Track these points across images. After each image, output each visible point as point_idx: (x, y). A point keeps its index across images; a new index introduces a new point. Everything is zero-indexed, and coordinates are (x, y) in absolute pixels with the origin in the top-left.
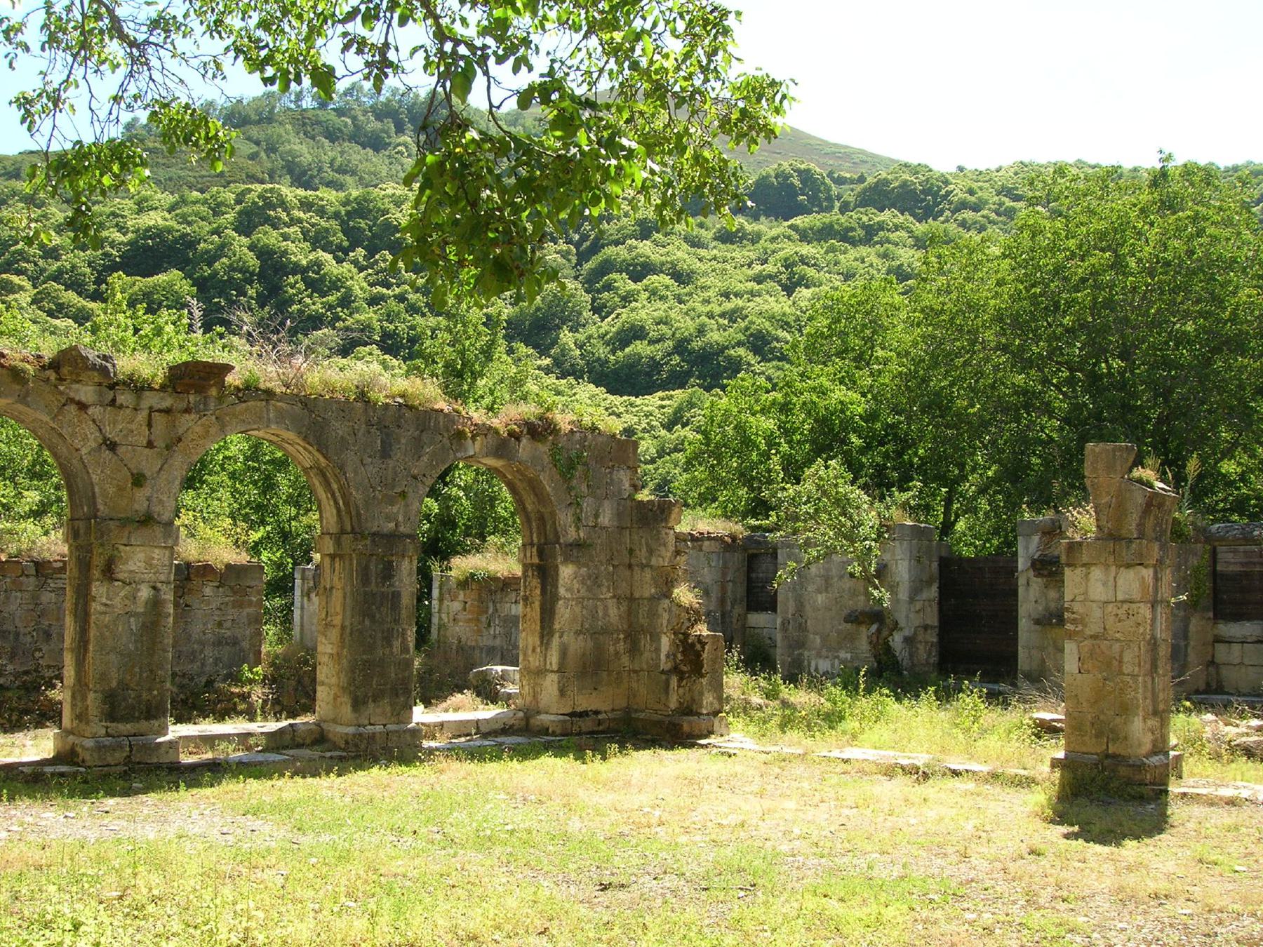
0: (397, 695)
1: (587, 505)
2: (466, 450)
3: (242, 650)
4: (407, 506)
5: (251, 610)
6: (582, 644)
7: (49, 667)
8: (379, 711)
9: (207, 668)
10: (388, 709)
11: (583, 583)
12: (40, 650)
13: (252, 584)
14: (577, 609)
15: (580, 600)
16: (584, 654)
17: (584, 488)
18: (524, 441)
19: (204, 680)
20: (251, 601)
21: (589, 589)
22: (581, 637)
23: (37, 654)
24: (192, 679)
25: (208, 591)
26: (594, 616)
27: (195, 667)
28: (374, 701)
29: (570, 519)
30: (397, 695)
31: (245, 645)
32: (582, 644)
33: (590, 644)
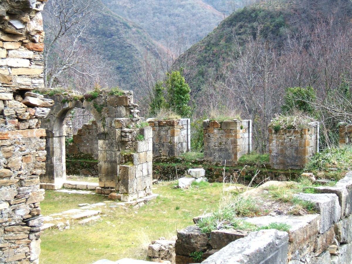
0: (50, 175)
1: (108, 120)
2: (66, 106)
3: (229, 153)
4: (50, 123)
5: (232, 138)
6: (107, 165)
7: (164, 155)
8: (46, 179)
9: (216, 160)
10: (48, 179)
11: (107, 145)
12: (161, 150)
13: (232, 129)
14: (105, 154)
15: (106, 151)
16: (108, 169)
17: (106, 114)
18: (84, 101)
19: (215, 163)
20: (232, 135)
21: (109, 148)
22: (107, 163)
23: (160, 151)
24: (211, 163)
25: (216, 131)
26: (111, 156)
27: (212, 158)
28: (44, 176)
29: (101, 125)
30: (50, 175)
31: (230, 151)
32: (107, 165)
33: (110, 166)
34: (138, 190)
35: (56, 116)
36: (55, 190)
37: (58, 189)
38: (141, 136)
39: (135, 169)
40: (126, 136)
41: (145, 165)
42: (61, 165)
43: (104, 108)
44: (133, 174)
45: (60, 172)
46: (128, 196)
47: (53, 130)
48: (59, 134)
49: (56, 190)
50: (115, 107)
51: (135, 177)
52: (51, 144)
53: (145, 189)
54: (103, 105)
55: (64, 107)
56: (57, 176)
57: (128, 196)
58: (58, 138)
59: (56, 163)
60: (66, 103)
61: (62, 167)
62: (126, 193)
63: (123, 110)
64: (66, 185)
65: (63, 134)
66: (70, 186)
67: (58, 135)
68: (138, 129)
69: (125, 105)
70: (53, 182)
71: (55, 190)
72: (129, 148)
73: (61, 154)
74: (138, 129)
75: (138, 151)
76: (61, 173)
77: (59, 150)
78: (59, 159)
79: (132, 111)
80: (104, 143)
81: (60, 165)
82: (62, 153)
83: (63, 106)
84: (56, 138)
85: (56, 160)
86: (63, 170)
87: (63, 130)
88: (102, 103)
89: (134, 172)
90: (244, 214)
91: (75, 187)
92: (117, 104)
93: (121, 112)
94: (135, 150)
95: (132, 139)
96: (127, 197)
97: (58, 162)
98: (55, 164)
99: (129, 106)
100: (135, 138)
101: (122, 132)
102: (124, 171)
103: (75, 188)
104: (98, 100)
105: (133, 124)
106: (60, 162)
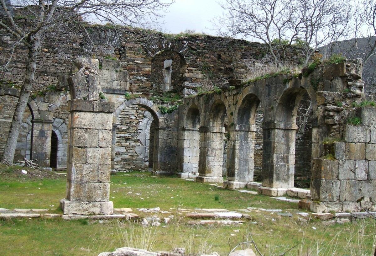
0: (270, 177)
34: (342, 199)
35: (278, 101)
36: (272, 196)
37: (277, 196)
38: (357, 119)
39: (337, 166)
40: (329, 115)
42: (287, 167)
43: (320, 83)
44: (332, 171)
45: (283, 174)
46: (319, 204)
47: (275, 119)
48: (285, 125)
49: (274, 196)
50: (331, 80)
51: (338, 177)
52: (273, 137)
53: (359, 201)
54: (319, 80)
55: (285, 89)
56: (278, 179)
57: (319, 204)
58: (283, 131)
59: (278, 162)
60: (287, 83)
61: (288, 170)
62: (317, 200)
63: (339, 83)
64: (289, 192)
65: (291, 127)
66: (293, 194)
67: (282, 126)
68: (354, 109)
69: (341, 75)
70: (271, 187)
71: (272, 196)
72: (335, 134)
74: (354, 109)
75: (346, 139)
76: (286, 177)
77: (284, 147)
78: (283, 159)
79: (349, 83)
81: (285, 166)
82: (289, 151)
83: (284, 88)
84: (280, 131)
85: (277, 158)
86: (290, 173)
87: (292, 122)
88: (318, 77)
89: (335, 170)
90: (117, 153)
91: (296, 195)
92: (332, 76)
93: (336, 85)
94: (342, 138)
95: (339, 121)
96: (317, 205)
97: (281, 162)
98: (275, 163)
99: (346, 76)
100: (345, 121)
101: (326, 110)
102: (318, 166)
103: (296, 197)
104: (315, 73)
105: (348, 101)
106: (284, 162)
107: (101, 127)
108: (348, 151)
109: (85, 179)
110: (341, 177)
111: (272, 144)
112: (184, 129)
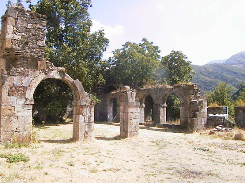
41: (203, 119)
73: (164, 115)
77: (163, 113)
80: (182, 108)
107: (136, 111)
108: (200, 115)
109: (132, 131)
110: (198, 124)
111: (159, 112)
112: (107, 106)
